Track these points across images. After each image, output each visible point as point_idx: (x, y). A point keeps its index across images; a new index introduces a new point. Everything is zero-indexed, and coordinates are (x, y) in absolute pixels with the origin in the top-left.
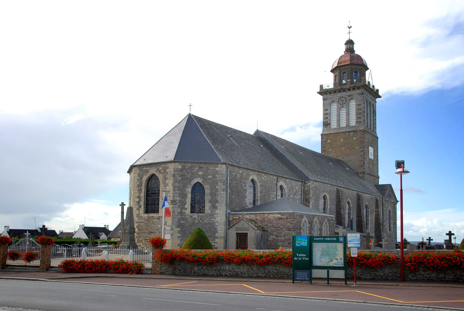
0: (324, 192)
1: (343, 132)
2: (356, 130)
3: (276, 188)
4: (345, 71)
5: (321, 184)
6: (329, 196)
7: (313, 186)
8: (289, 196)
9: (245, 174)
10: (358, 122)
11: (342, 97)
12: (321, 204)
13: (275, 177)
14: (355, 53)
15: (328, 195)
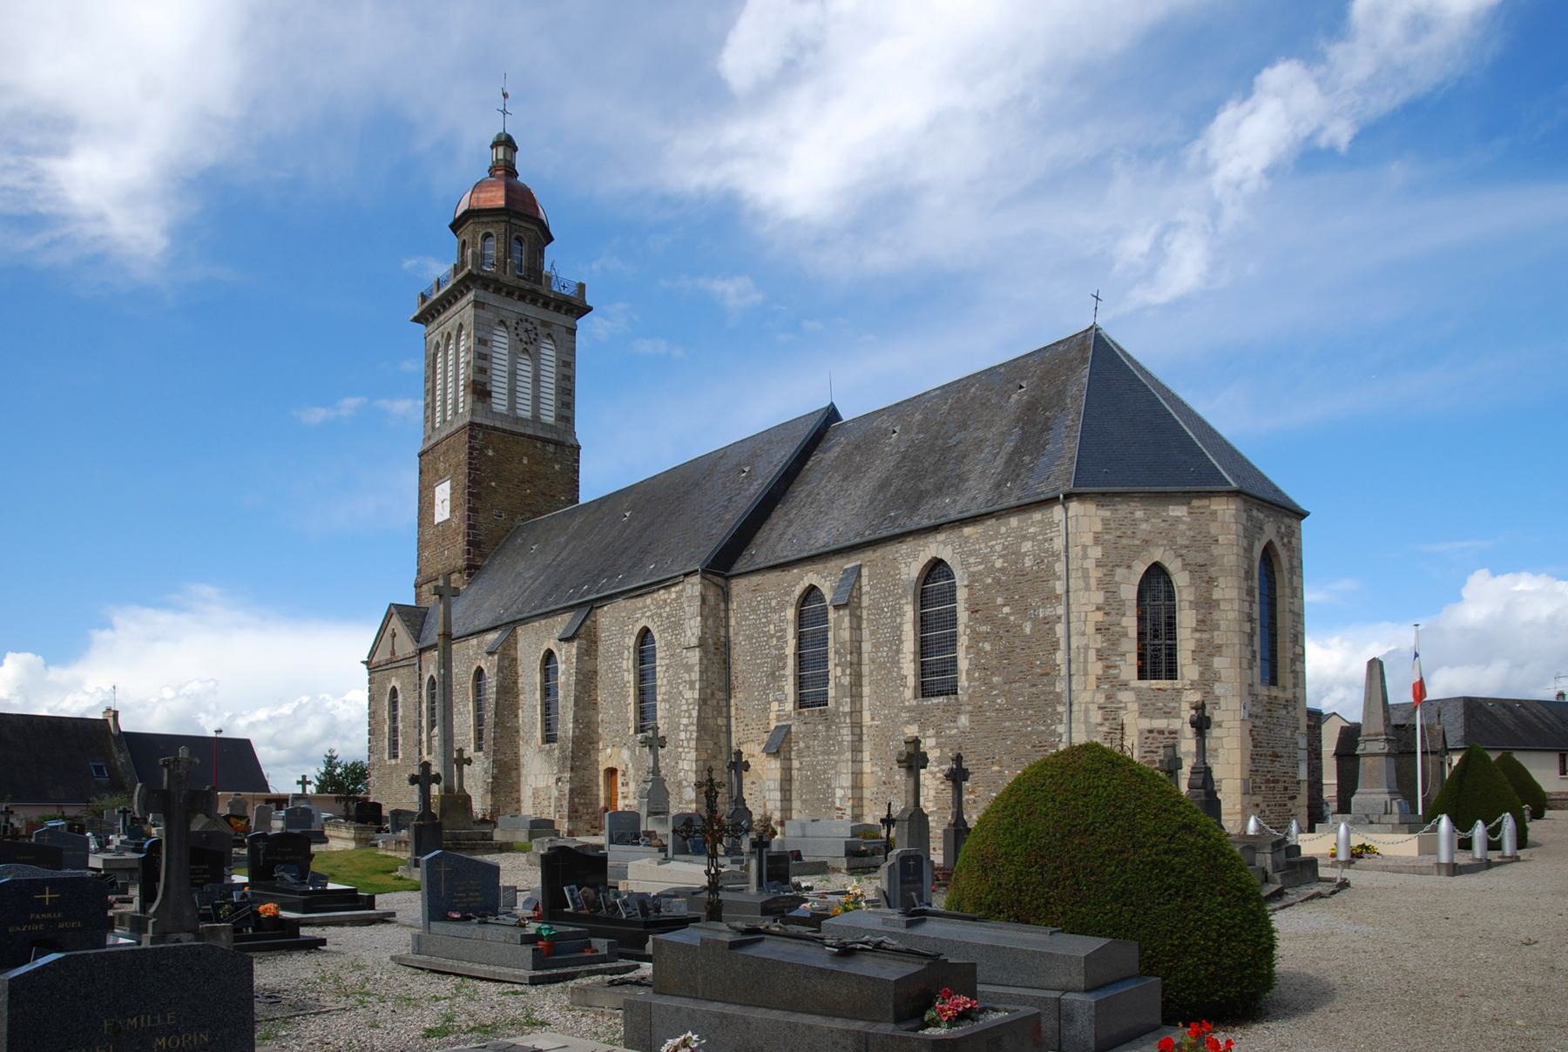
1: (529, 437)
2: (561, 439)
4: (490, 230)
10: (563, 417)
11: (526, 320)
14: (518, 179)
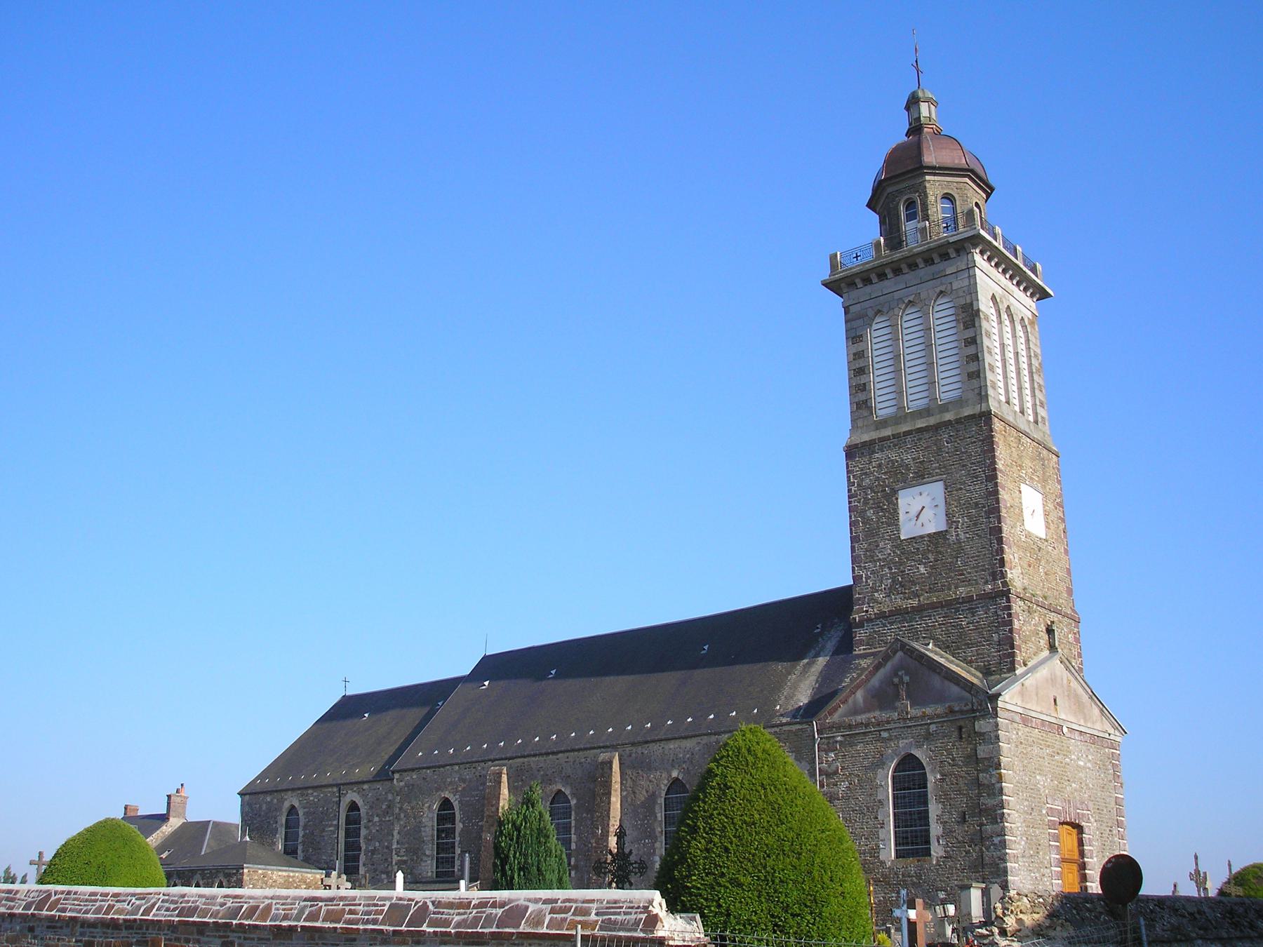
0: (438, 789)
3: (337, 810)
5: (428, 771)
6: (457, 797)
7: (402, 784)
8: (369, 821)
9: (275, 800)
12: (430, 824)
13: (335, 789)
15: (452, 795)
